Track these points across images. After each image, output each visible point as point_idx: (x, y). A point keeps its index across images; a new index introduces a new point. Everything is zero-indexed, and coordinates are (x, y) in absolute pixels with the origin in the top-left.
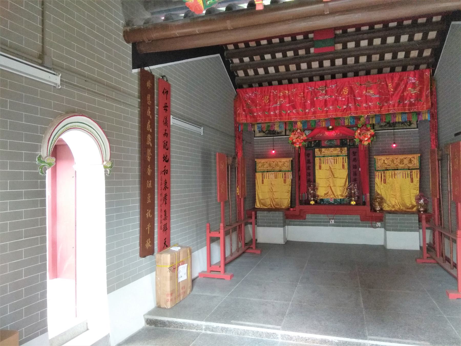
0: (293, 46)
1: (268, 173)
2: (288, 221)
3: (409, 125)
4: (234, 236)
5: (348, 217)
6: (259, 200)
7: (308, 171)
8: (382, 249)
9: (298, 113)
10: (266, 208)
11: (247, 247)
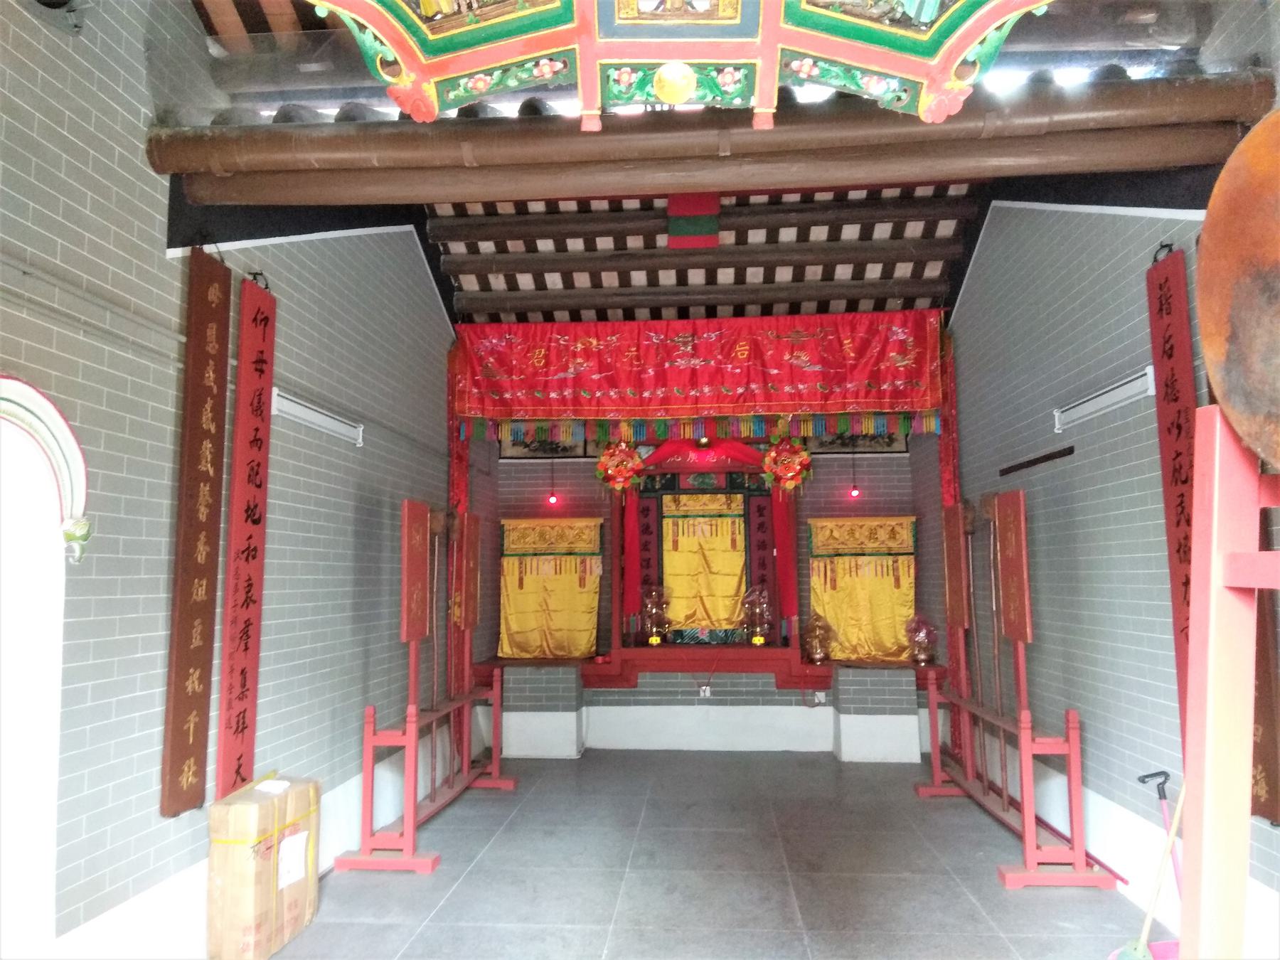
0: (612, 226)
1: (535, 559)
2: (588, 692)
3: (889, 445)
4: (442, 739)
5: (744, 678)
6: (510, 636)
7: (646, 555)
8: (829, 763)
9: (623, 399)
10: (528, 656)
11: (479, 771)
